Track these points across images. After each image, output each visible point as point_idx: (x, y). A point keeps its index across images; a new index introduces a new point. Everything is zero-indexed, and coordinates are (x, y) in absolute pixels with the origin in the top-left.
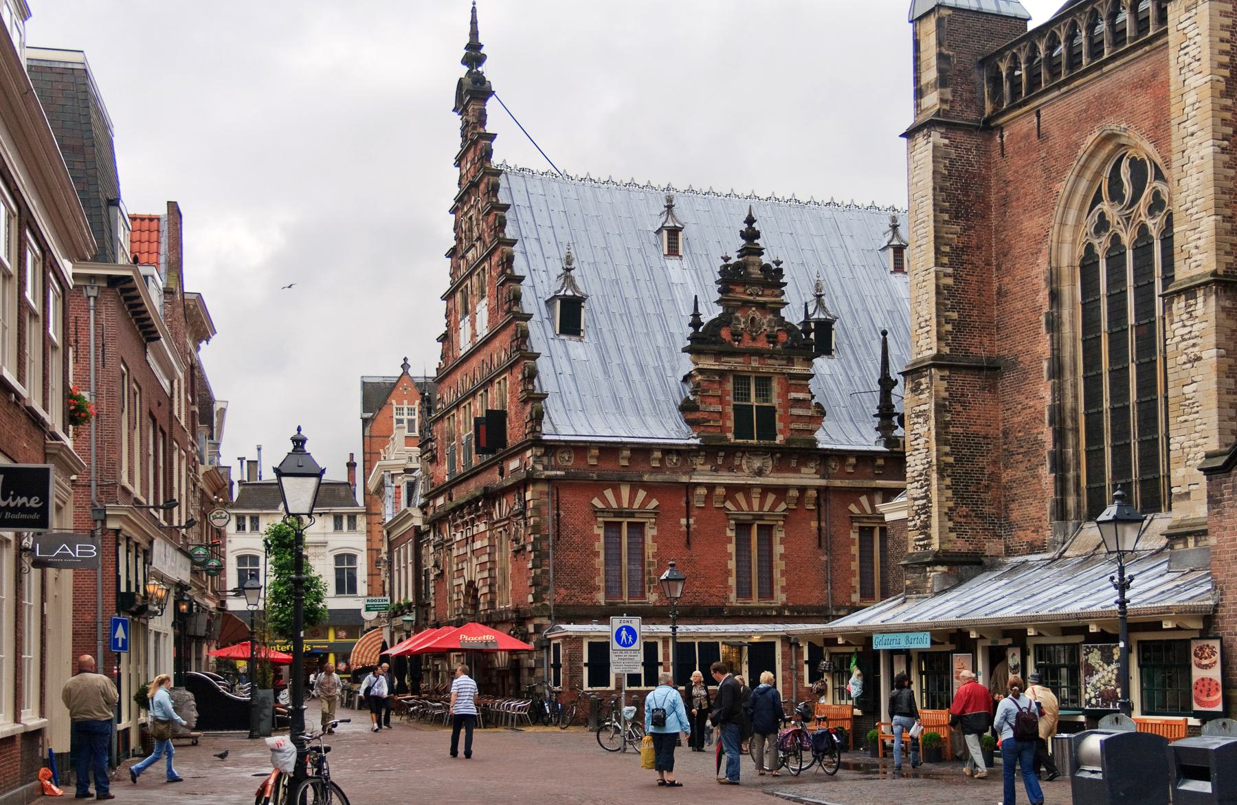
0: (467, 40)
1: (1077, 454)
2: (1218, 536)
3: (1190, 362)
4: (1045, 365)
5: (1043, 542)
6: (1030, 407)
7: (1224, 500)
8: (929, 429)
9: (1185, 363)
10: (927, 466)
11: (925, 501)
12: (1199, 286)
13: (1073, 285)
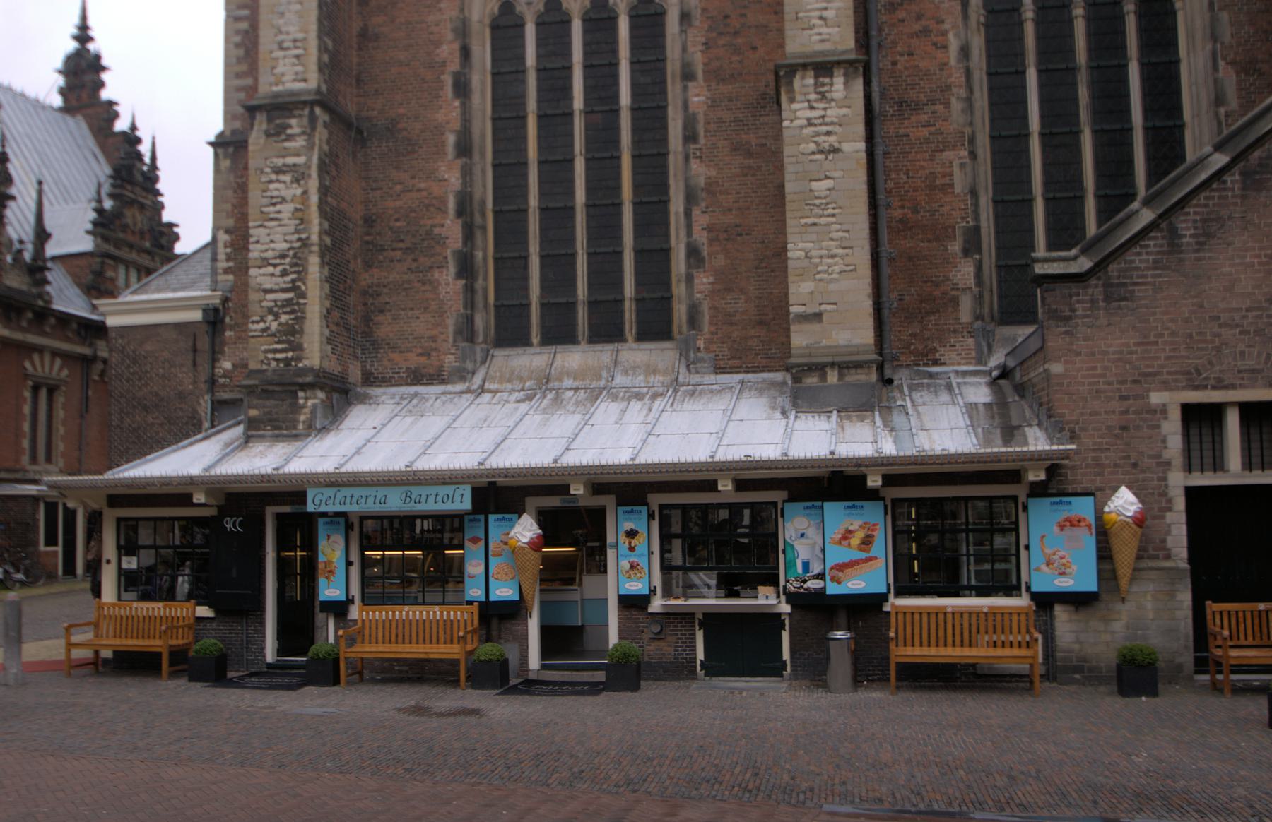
1: (485, 258)
2: (1066, 362)
3: (821, 152)
6: (419, 190)
7: (1077, 317)
8: (305, 192)
9: (813, 153)
10: (297, 245)
11: (290, 295)
12: (839, 63)
13: (484, 46)
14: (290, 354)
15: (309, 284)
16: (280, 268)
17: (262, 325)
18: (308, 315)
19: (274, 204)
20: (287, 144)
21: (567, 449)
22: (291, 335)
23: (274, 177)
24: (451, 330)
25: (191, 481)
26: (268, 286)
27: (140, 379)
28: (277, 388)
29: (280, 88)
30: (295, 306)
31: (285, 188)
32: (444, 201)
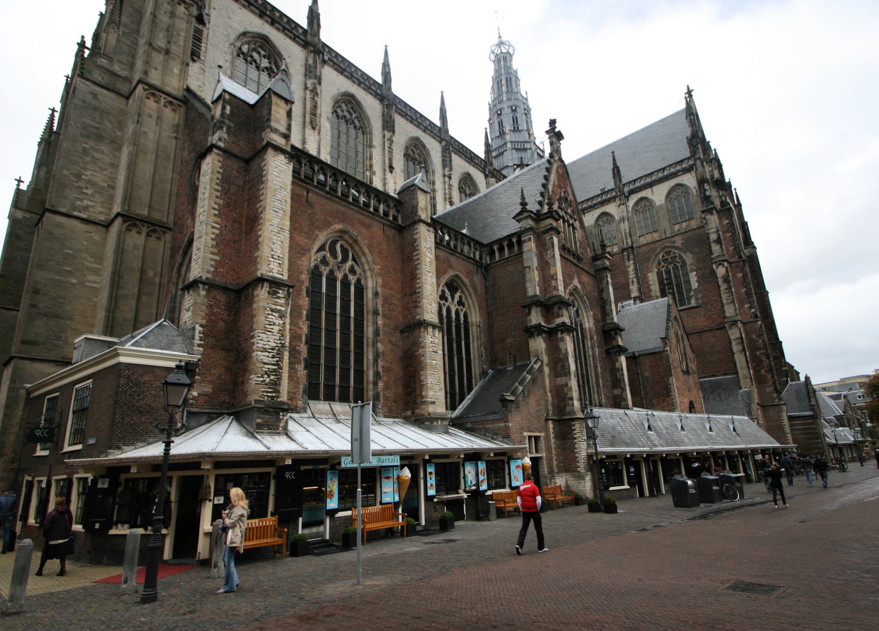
0: (382, 61)
4: (305, 312)
5: (296, 407)
8: (284, 323)
10: (280, 345)
11: (276, 367)
14: (274, 394)
15: (284, 364)
16: (272, 354)
17: (261, 379)
18: (283, 378)
19: (270, 325)
20: (277, 300)
21: (219, 442)
22: (275, 385)
23: (270, 313)
24: (301, 390)
25: (203, 456)
26: (266, 361)
27: (139, 395)
28: (271, 410)
29: (271, 274)
30: (277, 372)
31: (274, 318)
32: (301, 336)
